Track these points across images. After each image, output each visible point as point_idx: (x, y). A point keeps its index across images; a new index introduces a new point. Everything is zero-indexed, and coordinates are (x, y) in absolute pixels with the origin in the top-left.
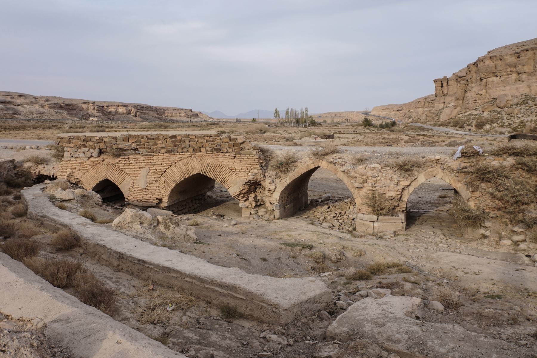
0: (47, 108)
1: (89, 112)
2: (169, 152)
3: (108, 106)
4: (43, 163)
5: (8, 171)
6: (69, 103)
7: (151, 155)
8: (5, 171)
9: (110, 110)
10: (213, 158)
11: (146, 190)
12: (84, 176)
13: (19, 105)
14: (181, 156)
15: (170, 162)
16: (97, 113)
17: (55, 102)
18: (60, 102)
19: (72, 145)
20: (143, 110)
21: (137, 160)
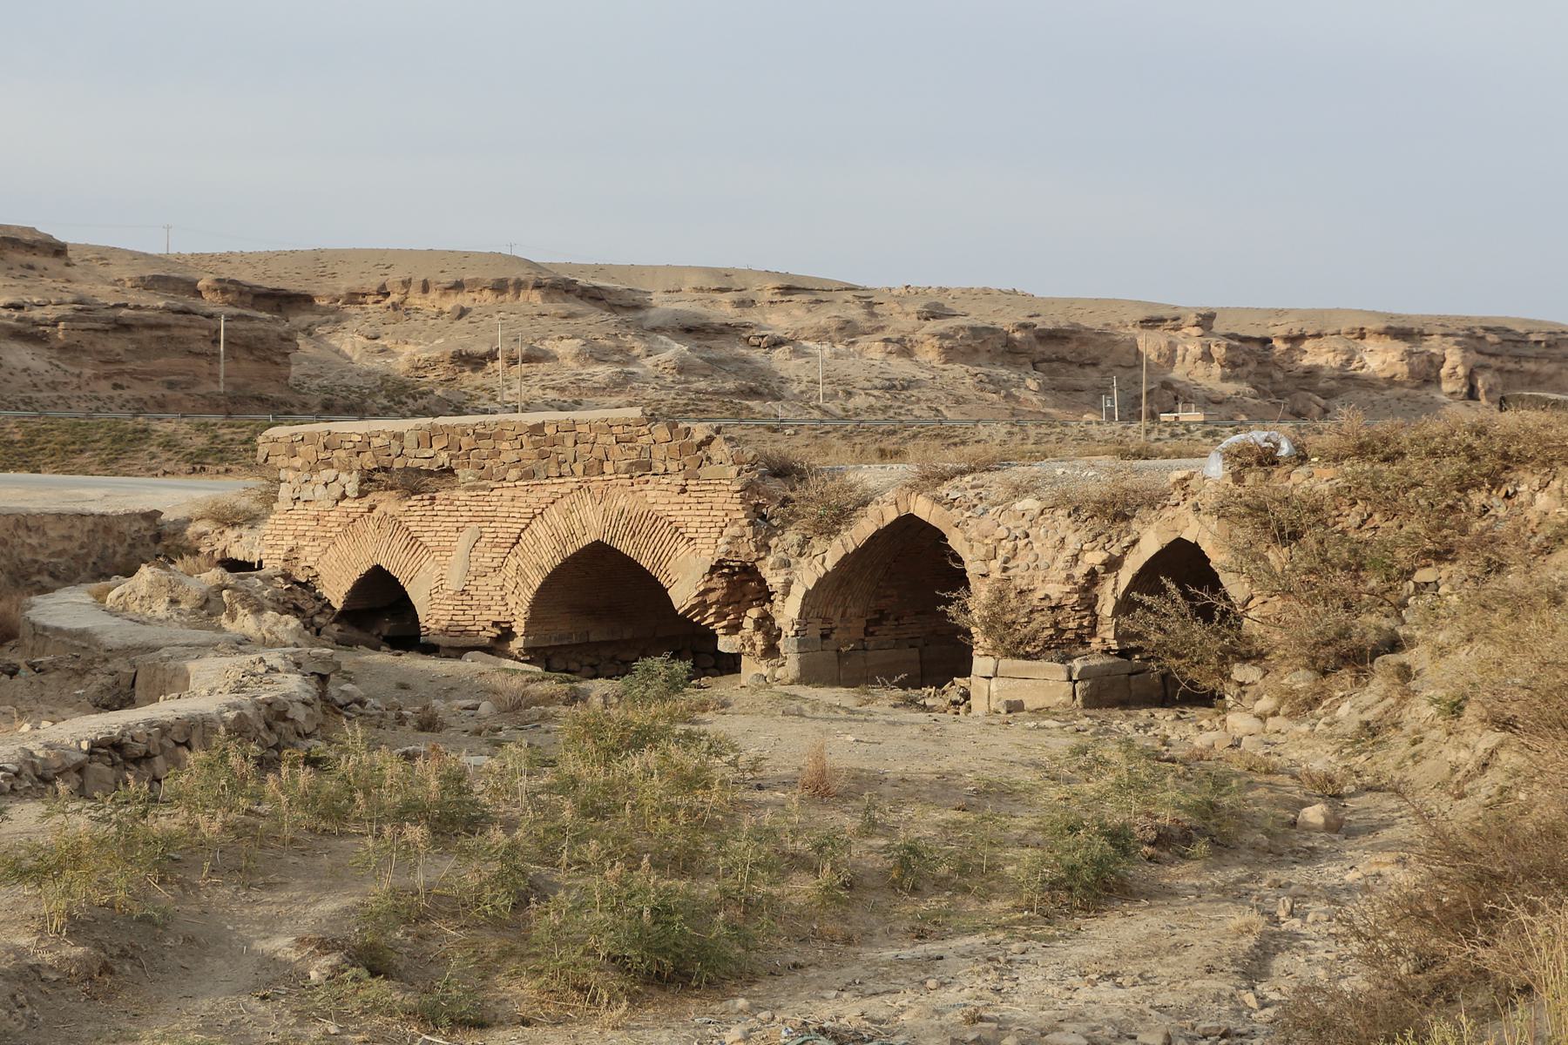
0: (929, 354)
1: (1178, 373)
2: (529, 475)
3: (1295, 340)
4: (240, 525)
5: (132, 546)
6: (1063, 324)
7: (483, 488)
8: (121, 545)
9: (1307, 361)
10: (633, 492)
11: (464, 597)
12: (326, 557)
13: (777, 343)
14: (555, 488)
16: (1225, 379)
17: (979, 316)
18: (1006, 321)
19: (298, 462)
20: (1519, 358)
21: (451, 504)
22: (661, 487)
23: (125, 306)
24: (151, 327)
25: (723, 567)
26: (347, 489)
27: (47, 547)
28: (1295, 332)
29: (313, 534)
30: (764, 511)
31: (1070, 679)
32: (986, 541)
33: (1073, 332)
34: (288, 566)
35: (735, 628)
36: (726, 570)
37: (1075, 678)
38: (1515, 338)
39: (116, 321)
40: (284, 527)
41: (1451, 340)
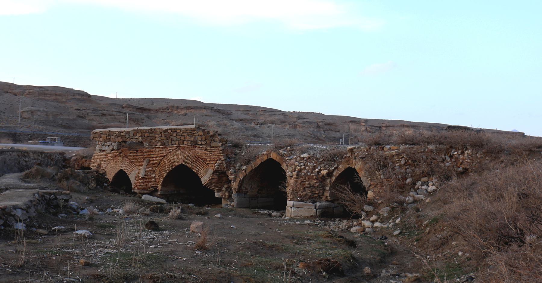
12: (108, 167)
19: (101, 139)
21: (142, 152)
22: (200, 148)
23: (104, 110)
25: (217, 172)
28: (388, 125)
32: (292, 166)
33: (334, 123)
36: (218, 173)
37: (317, 208)
39: (102, 114)
41: (425, 128)
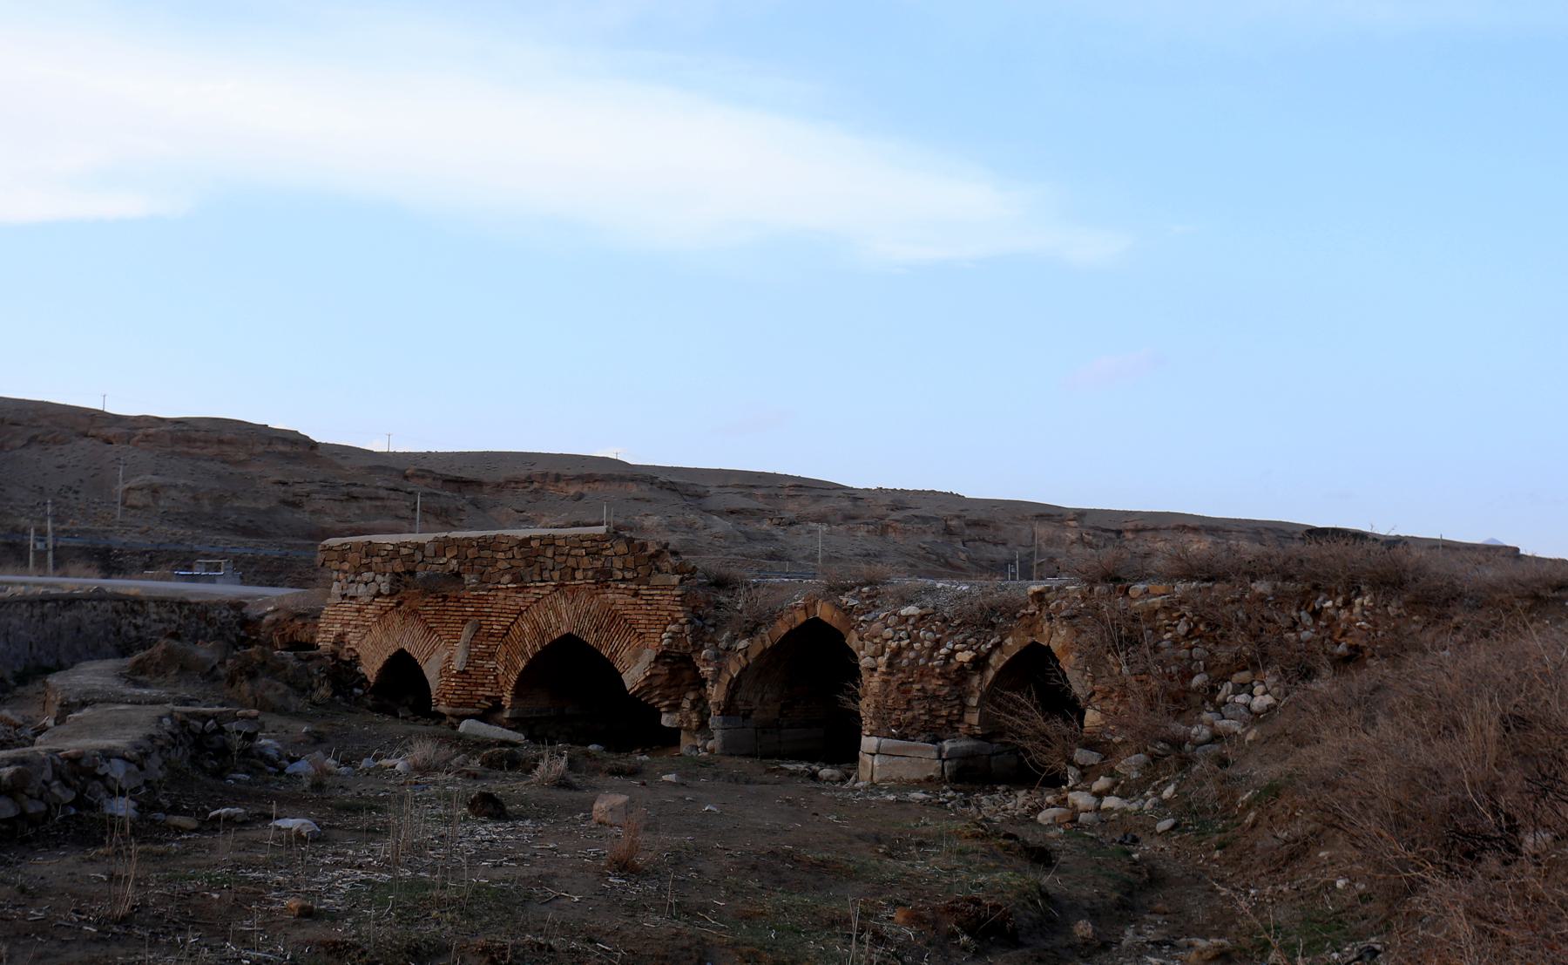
12: (365, 641)
15: (517, 605)
19: (346, 566)
21: (459, 601)
24: (370, 499)
25: (666, 657)
26: (382, 587)
27: (149, 628)
29: (355, 622)
30: (701, 612)
31: (940, 757)
34: (337, 648)
35: (675, 708)
36: (669, 660)
37: (944, 757)
38: (1284, 535)
39: (348, 494)
40: (334, 617)
41: (1244, 535)
